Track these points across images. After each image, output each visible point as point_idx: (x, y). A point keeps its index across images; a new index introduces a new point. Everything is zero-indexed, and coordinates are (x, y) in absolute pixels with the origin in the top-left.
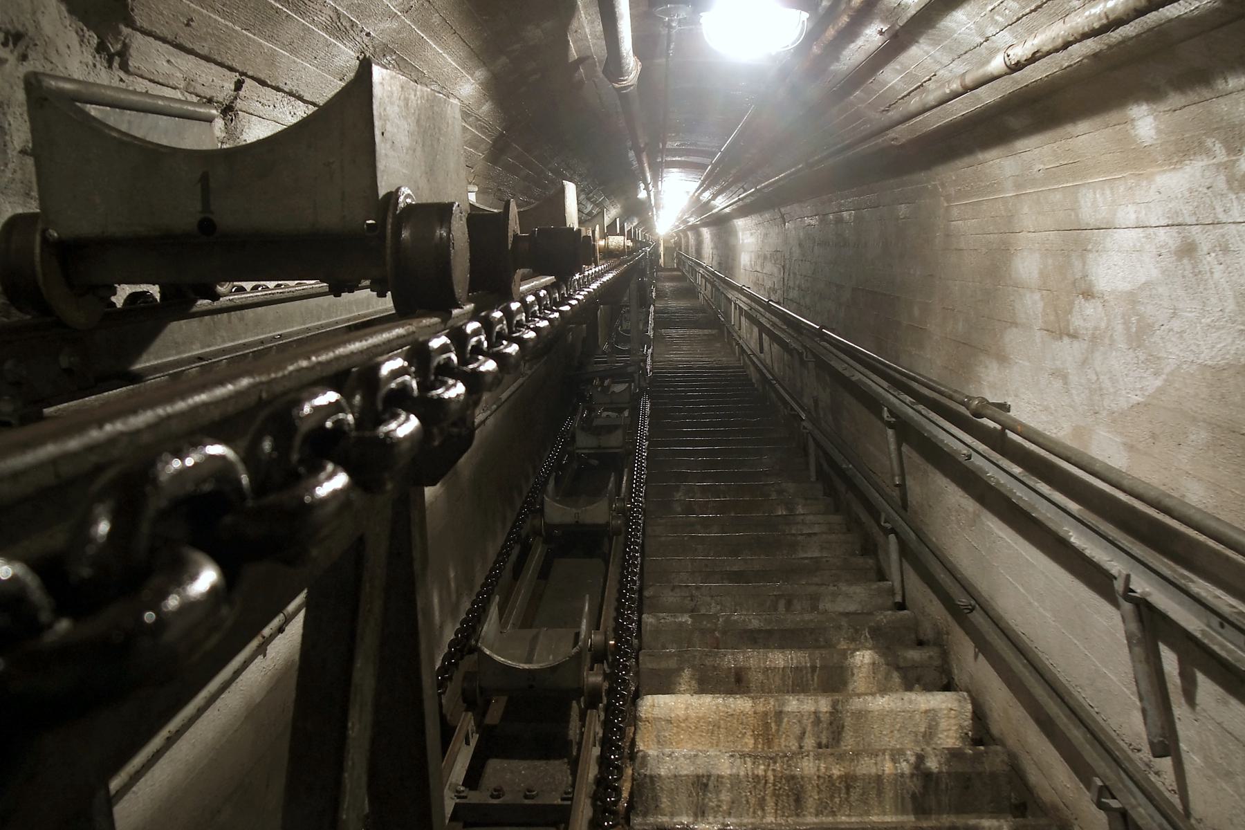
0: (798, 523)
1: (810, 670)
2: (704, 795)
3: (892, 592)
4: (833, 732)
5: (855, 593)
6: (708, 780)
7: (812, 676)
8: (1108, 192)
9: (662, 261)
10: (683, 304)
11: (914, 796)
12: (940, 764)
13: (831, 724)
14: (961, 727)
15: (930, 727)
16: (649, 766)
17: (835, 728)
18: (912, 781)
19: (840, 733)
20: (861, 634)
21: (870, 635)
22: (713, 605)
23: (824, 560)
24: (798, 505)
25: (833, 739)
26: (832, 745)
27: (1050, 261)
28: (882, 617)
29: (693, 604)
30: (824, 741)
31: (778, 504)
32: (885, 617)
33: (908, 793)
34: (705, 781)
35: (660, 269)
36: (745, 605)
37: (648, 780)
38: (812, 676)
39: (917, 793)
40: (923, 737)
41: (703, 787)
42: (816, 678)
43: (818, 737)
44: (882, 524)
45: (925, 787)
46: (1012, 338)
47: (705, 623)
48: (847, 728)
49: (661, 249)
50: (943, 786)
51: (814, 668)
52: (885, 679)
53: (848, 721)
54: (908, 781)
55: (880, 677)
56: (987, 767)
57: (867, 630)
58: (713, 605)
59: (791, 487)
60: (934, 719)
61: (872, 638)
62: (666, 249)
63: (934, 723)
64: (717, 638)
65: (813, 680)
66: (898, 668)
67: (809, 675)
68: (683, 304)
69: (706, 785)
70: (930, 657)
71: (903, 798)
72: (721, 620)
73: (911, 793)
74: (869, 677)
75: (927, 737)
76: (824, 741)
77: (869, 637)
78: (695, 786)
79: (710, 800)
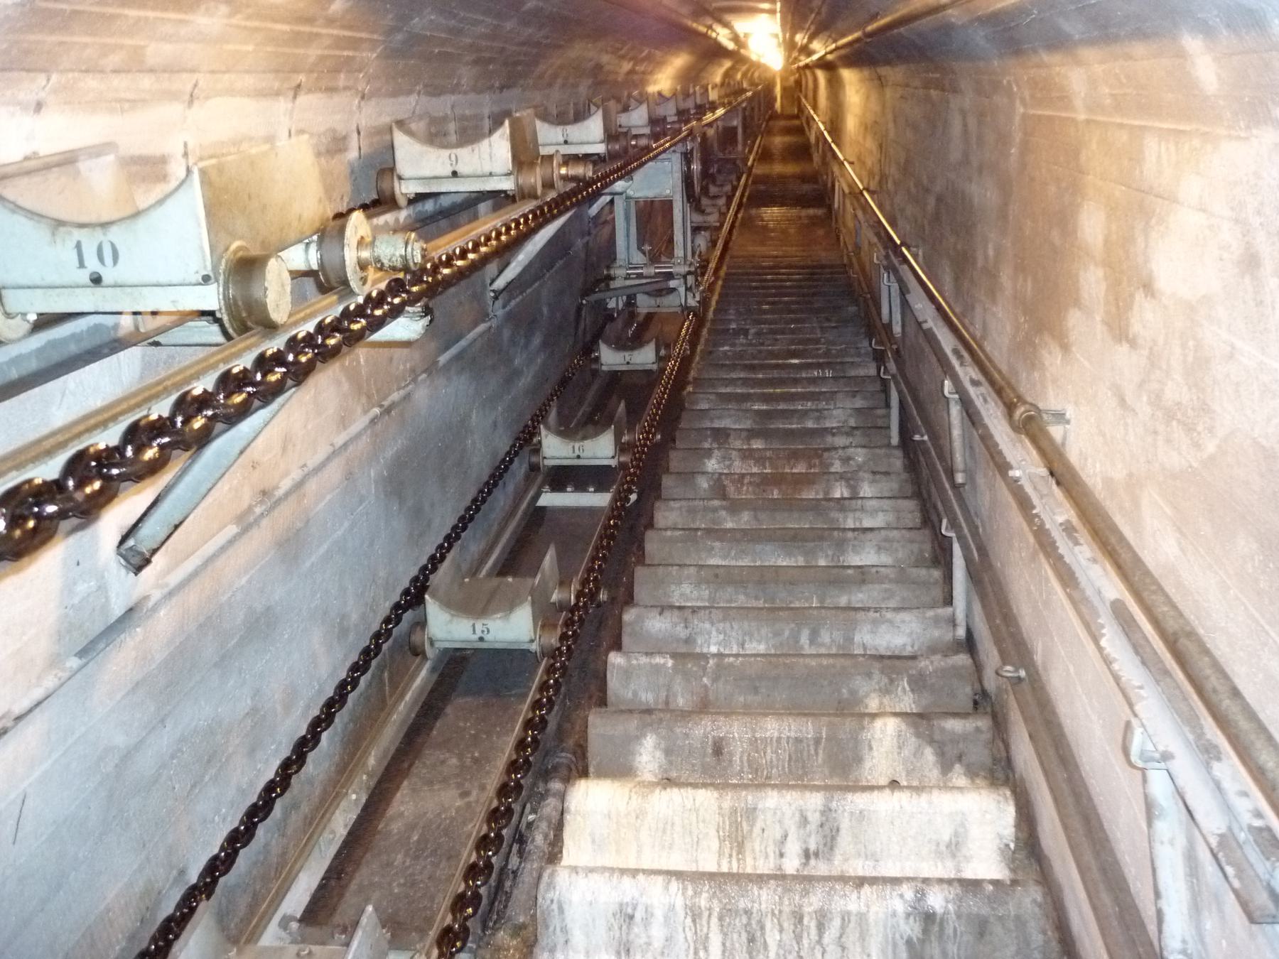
0: (856, 510)
1: (812, 742)
2: (629, 928)
3: (953, 622)
4: (825, 837)
5: (903, 622)
6: (635, 909)
7: (816, 751)
8: (1172, 148)
9: (778, 105)
10: (790, 169)
11: (909, 942)
12: (947, 902)
13: (822, 825)
14: (1000, 837)
15: (956, 834)
16: (557, 888)
17: (828, 832)
18: (907, 923)
19: (833, 838)
20: (898, 686)
21: (910, 686)
22: (714, 633)
23: (874, 570)
24: (863, 481)
25: (825, 845)
26: (823, 852)
27: (1114, 227)
28: (927, 662)
29: (688, 632)
30: (812, 847)
31: (837, 481)
32: (932, 662)
33: (902, 938)
34: (630, 911)
35: (774, 116)
36: (756, 635)
37: (555, 906)
38: (816, 751)
39: (915, 939)
40: (947, 847)
41: (627, 920)
42: (821, 752)
43: (805, 842)
44: (943, 532)
45: (926, 931)
46: (1074, 319)
47: (690, 666)
48: (843, 832)
49: (778, 91)
50: (949, 931)
51: (817, 741)
52: (915, 755)
53: (845, 824)
54: (902, 922)
55: (906, 752)
56: (1011, 909)
57: (905, 680)
58: (714, 633)
59: (860, 456)
60: (963, 825)
61: (912, 690)
62: (784, 89)
63: (962, 830)
64: (706, 686)
65: (817, 754)
66: (931, 741)
67: (812, 748)
68: (790, 169)
69: (632, 917)
70: (978, 730)
71: (895, 945)
72: (711, 662)
73: (905, 937)
74: (892, 753)
75: (953, 847)
76: (812, 847)
77: (908, 689)
78: (618, 916)
79: (637, 936)
